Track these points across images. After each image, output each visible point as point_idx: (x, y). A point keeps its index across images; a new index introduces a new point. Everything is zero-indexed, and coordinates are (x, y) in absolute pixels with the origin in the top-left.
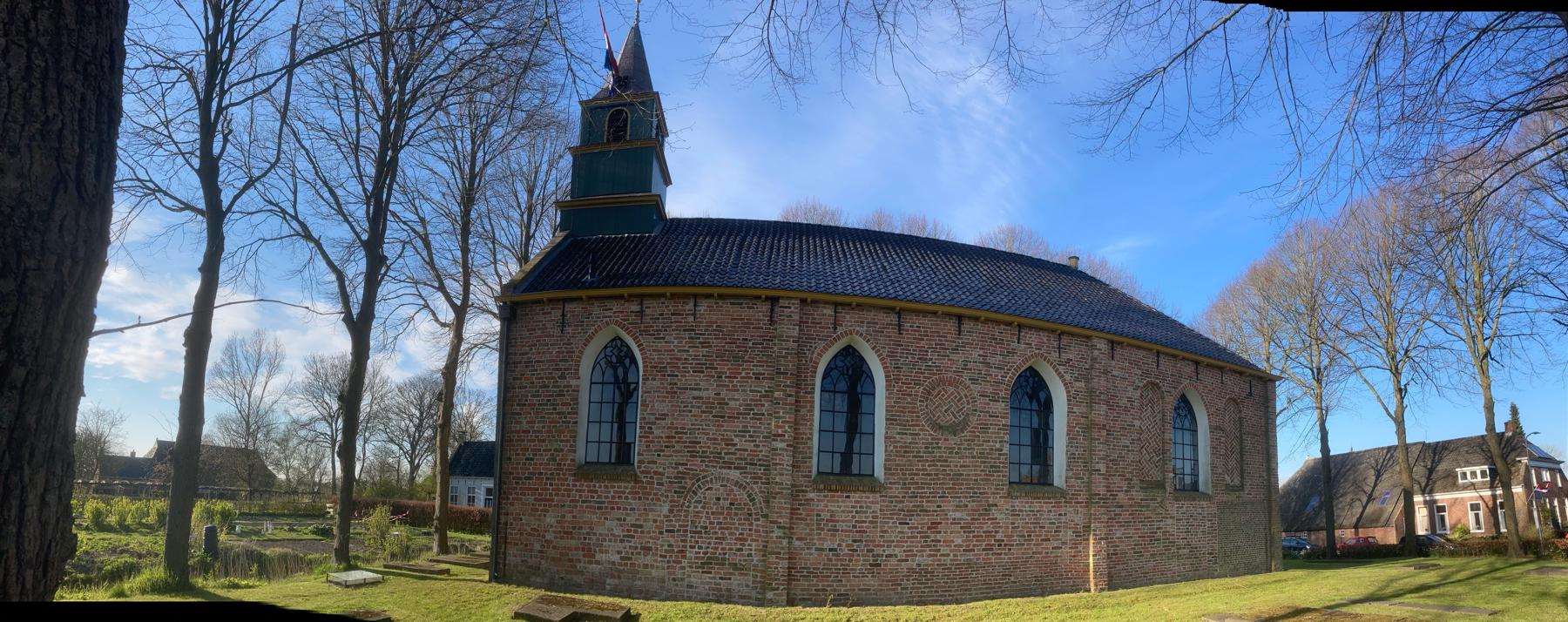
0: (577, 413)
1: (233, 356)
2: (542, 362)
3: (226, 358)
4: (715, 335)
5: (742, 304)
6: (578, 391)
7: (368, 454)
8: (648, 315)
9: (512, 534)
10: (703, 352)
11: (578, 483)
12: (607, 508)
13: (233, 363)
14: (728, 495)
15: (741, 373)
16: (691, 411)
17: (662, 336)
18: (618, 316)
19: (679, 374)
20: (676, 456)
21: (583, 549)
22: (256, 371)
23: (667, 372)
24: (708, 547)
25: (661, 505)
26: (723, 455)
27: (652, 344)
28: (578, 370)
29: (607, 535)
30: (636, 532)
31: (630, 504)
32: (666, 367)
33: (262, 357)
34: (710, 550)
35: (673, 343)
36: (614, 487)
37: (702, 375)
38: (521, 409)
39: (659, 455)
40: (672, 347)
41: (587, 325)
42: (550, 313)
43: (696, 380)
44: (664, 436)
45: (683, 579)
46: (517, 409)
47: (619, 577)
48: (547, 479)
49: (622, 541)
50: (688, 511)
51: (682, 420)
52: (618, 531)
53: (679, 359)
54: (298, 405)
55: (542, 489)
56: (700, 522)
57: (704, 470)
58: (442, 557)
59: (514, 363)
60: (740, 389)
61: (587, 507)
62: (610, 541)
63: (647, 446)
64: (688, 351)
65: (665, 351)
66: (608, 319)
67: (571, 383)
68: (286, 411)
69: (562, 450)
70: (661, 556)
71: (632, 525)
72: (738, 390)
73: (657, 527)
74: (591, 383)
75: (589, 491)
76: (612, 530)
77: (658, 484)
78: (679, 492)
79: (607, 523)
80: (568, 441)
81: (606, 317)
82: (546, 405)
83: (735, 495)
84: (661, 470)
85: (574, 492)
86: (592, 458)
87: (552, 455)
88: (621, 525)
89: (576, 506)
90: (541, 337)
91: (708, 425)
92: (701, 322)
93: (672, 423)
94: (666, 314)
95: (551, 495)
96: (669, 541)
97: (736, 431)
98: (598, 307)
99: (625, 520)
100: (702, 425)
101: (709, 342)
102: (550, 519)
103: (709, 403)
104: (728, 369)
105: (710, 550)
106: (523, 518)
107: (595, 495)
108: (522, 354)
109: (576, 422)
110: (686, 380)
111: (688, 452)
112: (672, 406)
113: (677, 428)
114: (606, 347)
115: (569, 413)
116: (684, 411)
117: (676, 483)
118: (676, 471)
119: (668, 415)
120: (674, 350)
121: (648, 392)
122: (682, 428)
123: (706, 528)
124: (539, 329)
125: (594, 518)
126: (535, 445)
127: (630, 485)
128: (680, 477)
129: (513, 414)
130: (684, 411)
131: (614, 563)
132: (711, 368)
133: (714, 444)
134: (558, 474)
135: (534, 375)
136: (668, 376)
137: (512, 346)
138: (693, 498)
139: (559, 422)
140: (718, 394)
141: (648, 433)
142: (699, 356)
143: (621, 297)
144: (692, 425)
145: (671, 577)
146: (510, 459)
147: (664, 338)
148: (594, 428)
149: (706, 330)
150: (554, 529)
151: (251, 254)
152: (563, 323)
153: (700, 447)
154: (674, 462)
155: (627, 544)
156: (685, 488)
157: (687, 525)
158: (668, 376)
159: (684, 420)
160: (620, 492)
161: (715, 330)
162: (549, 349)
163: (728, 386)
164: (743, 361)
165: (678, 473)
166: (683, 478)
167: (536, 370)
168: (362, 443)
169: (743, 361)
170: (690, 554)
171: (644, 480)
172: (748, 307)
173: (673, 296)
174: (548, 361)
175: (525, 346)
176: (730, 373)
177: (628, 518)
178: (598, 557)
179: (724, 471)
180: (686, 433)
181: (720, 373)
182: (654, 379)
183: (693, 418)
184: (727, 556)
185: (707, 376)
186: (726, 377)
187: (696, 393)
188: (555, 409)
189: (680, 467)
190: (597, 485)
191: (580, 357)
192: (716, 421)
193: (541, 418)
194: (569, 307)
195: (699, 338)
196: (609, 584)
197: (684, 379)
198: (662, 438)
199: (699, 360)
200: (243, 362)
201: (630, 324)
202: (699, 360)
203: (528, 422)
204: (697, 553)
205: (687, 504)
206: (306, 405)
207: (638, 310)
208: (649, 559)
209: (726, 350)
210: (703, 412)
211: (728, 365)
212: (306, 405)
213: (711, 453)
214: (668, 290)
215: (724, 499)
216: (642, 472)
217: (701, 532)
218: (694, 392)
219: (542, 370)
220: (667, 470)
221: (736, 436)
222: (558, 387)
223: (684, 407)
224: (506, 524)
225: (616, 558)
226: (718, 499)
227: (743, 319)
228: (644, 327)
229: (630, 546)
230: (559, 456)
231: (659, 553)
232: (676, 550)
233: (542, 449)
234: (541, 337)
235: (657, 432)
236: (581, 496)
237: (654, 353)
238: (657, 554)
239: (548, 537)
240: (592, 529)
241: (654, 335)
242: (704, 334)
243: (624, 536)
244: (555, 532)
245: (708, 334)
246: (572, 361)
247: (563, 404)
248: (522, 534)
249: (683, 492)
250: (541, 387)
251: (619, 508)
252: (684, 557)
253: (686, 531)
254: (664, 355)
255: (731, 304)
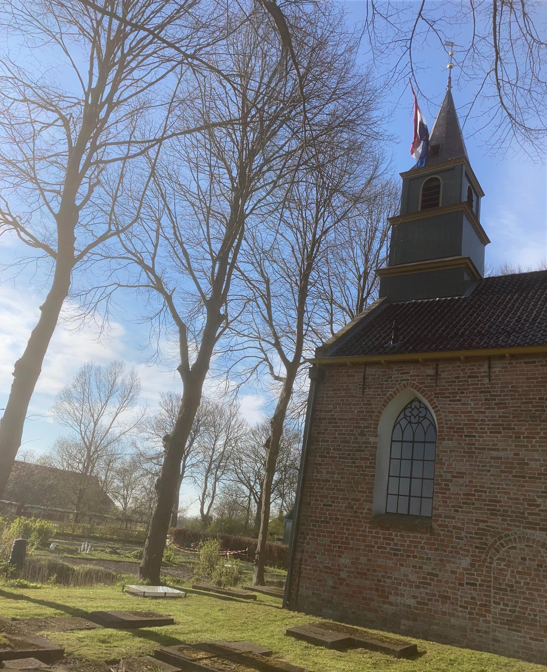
0: (374, 468)
1: (85, 383)
2: (343, 419)
3: (79, 385)
4: (511, 395)
5: (534, 362)
6: (376, 448)
7: (218, 491)
8: (444, 379)
9: (306, 569)
10: (499, 413)
11: (374, 531)
12: (402, 555)
13: (84, 390)
14: (534, 556)
15: (539, 433)
16: (489, 471)
17: (458, 398)
18: (415, 380)
19: (477, 435)
20: (476, 513)
21: (377, 590)
22: (107, 401)
23: (464, 432)
24: (515, 606)
25: (460, 559)
26: (526, 515)
27: (447, 406)
28: (377, 428)
29: (403, 580)
30: (432, 580)
31: (426, 554)
32: (463, 428)
33: (115, 388)
34: (517, 609)
35: (471, 404)
36: (410, 537)
37: (499, 435)
38: (322, 461)
39: (457, 511)
40: (469, 409)
41: (386, 388)
42: (354, 376)
43: (493, 441)
44: (462, 493)
45: (486, 632)
46: (319, 460)
47: (415, 620)
48: (344, 524)
49: (417, 587)
50: (491, 568)
51: (480, 478)
52: (413, 578)
53: (477, 420)
54: (147, 439)
55: (338, 533)
56: (504, 580)
57: (506, 529)
58: (259, 587)
59: (320, 419)
60: (540, 449)
61: (382, 552)
62: (405, 585)
63: (444, 502)
64: (484, 413)
65: (462, 413)
66: (405, 382)
67: (370, 440)
68: (134, 444)
69: (359, 500)
70: (461, 606)
71: (429, 574)
72: (538, 451)
73: (456, 578)
74: (392, 441)
75: (384, 538)
76: (408, 575)
77: (457, 538)
78: (480, 548)
79: (403, 569)
80: (364, 492)
81: (404, 380)
82: (347, 458)
83: (543, 557)
84: (459, 525)
85: (370, 538)
86: (392, 509)
87: (350, 503)
88: (417, 573)
89: (372, 551)
90: (344, 397)
91: (508, 485)
92: (496, 383)
93: (471, 482)
94: (463, 377)
95: (347, 538)
96: (471, 594)
97: (538, 492)
98: (396, 370)
99: (421, 568)
100: (502, 485)
101: (505, 403)
102: (345, 560)
103: (508, 463)
104: (525, 429)
105: (517, 609)
106: (317, 556)
107: (392, 543)
108: (326, 411)
109: (373, 476)
110: (483, 441)
111: (488, 509)
112: (471, 465)
113: (476, 486)
114: (405, 409)
115: (366, 467)
116: (483, 470)
117: (477, 538)
118: (476, 527)
119: (465, 474)
120: (471, 412)
121: (445, 452)
122: (481, 487)
123: (512, 586)
124: (343, 390)
125: (390, 563)
126: (334, 494)
127: (425, 536)
128: (480, 534)
129: (315, 464)
130: (483, 470)
131: (409, 606)
132: (508, 429)
133: (517, 504)
134: (355, 521)
135: (336, 431)
136: (466, 436)
137: (320, 404)
138: (495, 556)
139: (357, 475)
140: (518, 454)
141: (445, 489)
142: (495, 417)
143: (416, 362)
144: (491, 484)
145: (475, 628)
146: (310, 504)
147: (460, 400)
148: (394, 482)
149: (501, 391)
150: (347, 569)
151: (104, 295)
152: (364, 385)
153: (501, 506)
154: (474, 519)
155: (422, 590)
156: (486, 544)
157: (490, 582)
158: (466, 436)
159: (483, 479)
160: (415, 542)
161: (511, 391)
162: (352, 408)
163: (527, 446)
164: (541, 421)
165: (479, 529)
166: (485, 535)
167: (339, 427)
168: (213, 481)
169: (541, 421)
170: (496, 609)
171: (442, 533)
172: (541, 366)
173: (468, 359)
174: (350, 419)
175: (330, 404)
176: (528, 433)
177: (425, 567)
178: (392, 598)
179: (530, 531)
180: (485, 492)
181: (517, 433)
182: (450, 440)
183: (492, 478)
184: (537, 618)
185: (504, 437)
186: (524, 437)
187: (494, 453)
188: (354, 463)
189: (480, 524)
190: (394, 533)
191: (379, 417)
192: (517, 481)
193: (341, 469)
194: (370, 371)
195: (495, 400)
196: (404, 625)
197: (481, 439)
198: (460, 495)
199: (495, 421)
200: (95, 391)
201: (426, 387)
202: (495, 421)
203: (328, 473)
204: (502, 609)
205: (489, 560)
206: (156, 440)
207: (434, 374)
208: (446, 608)
209: (523, 411)
210: (502, 472)
211: (525, 425)
212: (156, 440)
213: (513, 512)
214: (462, 354)
215: (531, 560)
216: (440, 525)
217: (506, 590)
218: (493, 453)
219: (344, 426)
220: (466, 525)
221: (538, 497)
222: (358, 443)
223: (483, 466)
224: (301, 560)
225: (412, 602)
226: (524, 559)
227: (538, 378)
228: (440, 390)
229: (426, 593)
230: (355, 504)
231: (459, 604)
232: (479, 603)
233: (340, 497)
234: (344, 397)
235: (453, 489)
236: (376, 543)
237: (450, 415)
238: (457, 604)
239: (343, 575)
240: (386, 572)
241: (450, 397)
242: (500, 396)
243: (420, 582)
244: (349, 572)
245: (504, 395)
246: (372, 420)
247: (361, 459)
248: (315, 571)
249: (485, 549)
250: (342, 442)
251: (415, 557)
252: (489, 611)
253: (489, 586)
254: (461, 416)
255: (525, 363)
